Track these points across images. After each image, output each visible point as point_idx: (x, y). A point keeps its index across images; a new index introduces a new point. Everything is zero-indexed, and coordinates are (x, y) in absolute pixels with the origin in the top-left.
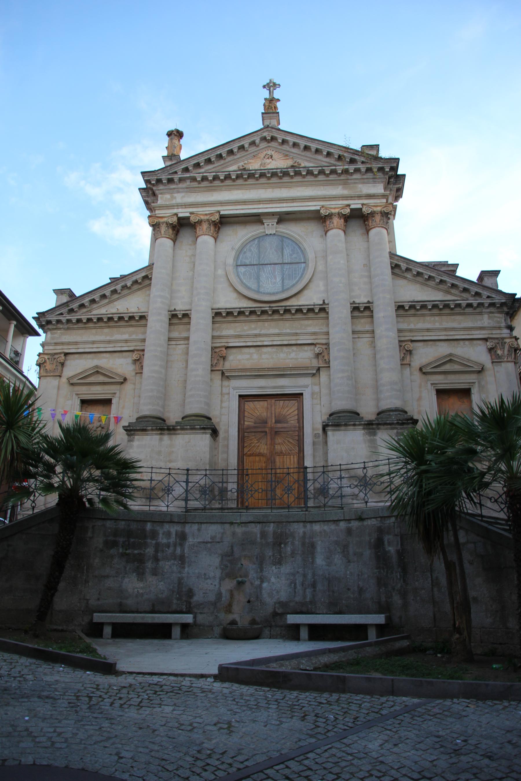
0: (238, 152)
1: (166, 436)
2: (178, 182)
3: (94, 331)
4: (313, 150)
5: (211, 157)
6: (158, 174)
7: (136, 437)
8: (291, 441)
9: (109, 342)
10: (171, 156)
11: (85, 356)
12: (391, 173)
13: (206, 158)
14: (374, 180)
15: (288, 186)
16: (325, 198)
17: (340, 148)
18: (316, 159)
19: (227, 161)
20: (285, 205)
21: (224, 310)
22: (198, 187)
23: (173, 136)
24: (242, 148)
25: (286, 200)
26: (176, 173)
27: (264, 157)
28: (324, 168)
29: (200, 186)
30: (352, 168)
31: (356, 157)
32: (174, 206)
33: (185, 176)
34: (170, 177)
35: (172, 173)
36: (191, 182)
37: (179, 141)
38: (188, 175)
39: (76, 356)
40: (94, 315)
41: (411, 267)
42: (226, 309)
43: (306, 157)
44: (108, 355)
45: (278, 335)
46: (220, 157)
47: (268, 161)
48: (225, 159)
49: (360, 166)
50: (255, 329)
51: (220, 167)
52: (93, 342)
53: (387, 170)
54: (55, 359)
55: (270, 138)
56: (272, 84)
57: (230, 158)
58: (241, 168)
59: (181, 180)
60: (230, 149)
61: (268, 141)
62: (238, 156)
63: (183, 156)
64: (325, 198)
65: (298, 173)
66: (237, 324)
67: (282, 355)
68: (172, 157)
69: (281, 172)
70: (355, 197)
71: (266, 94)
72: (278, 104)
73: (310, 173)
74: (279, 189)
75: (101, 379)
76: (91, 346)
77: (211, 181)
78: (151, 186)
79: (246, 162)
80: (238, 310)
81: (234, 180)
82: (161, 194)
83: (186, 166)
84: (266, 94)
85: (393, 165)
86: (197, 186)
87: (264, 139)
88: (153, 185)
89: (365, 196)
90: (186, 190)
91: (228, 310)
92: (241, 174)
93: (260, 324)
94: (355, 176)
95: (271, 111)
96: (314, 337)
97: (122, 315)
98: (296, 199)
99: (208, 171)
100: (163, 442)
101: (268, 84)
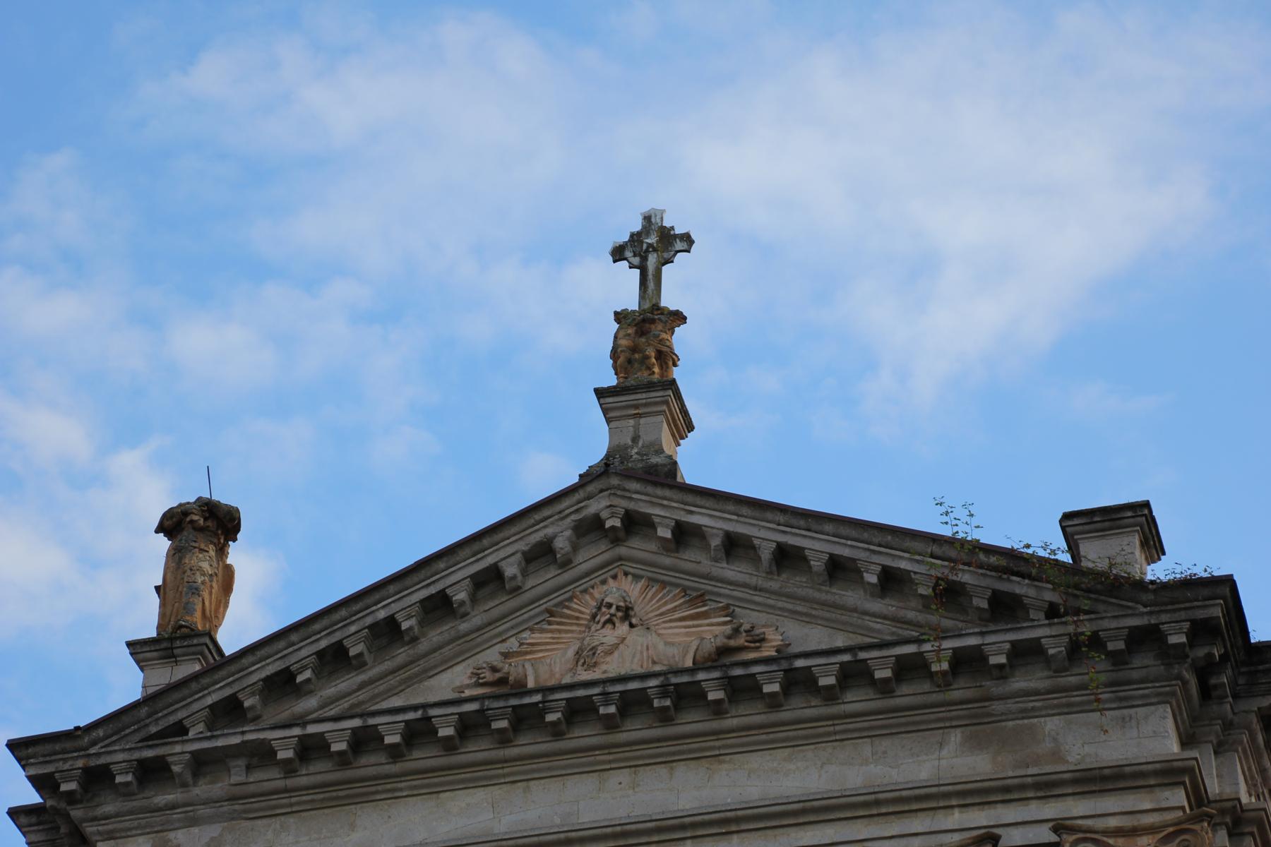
0: (474, 599)
2: (190, 779)
4: (817, 564)
5: (338, 639)
6: (94, 743)
10: (171, 639)
12: (1201, 652)
13: (323, 644)
14: (1123, 695)
15: (707, 750)
16: (878, 803)
17: (936, 549)
18: (835, 606)
19: (423, 646)
22: (286, 790)
23: (187, 533)
24: (490, 580)
25: (694, 826)
26: (180, 730)
27: (594, 616)
28: (862, 655)
29: (290, 782)
30: (997, 645)
31: (1019, 587)
33: (220, 743)
34: (149, 753)
35: (162, 734)
36: (249, 768)
37: (222, 551)
38: (236, 740)
46: (388, 632)
47: (608, 636)
48: (414, 640)
49: (1040, 631)
51: (362, 696)
53: (1177, 639)
55: (617, 523)
56: (652, 239)
57: (436, 635)
58: (489, 676)
59: (202, 764)
60: (433, 590)
61: (615, 538)
62: (477, 620)
63: (240, 627)
64: (878, 803)
65: (742, 690)
68: (179, 637)
69: (664, 691)
70: (1023, 787)
71: (624, 287)
72: (681, 339)
73: (799, 682)
74: (662, 771)
77: (343, 760)
78: (63, 805)
79: (513, 644)
81: (449, 746)
82: (110, 836)
83: (228, 692)
84: (624, 287)
85: (1201, 614)
86: (280, 784)
87: (591, 528)
88: (70, 797)
89: (1075, 782)
90: (226, 807)
92: (481, 712)
94: (1019, 683)
95: (643, 376)
98: (738, 820)
99: (326, 708)
101: (636, 238)
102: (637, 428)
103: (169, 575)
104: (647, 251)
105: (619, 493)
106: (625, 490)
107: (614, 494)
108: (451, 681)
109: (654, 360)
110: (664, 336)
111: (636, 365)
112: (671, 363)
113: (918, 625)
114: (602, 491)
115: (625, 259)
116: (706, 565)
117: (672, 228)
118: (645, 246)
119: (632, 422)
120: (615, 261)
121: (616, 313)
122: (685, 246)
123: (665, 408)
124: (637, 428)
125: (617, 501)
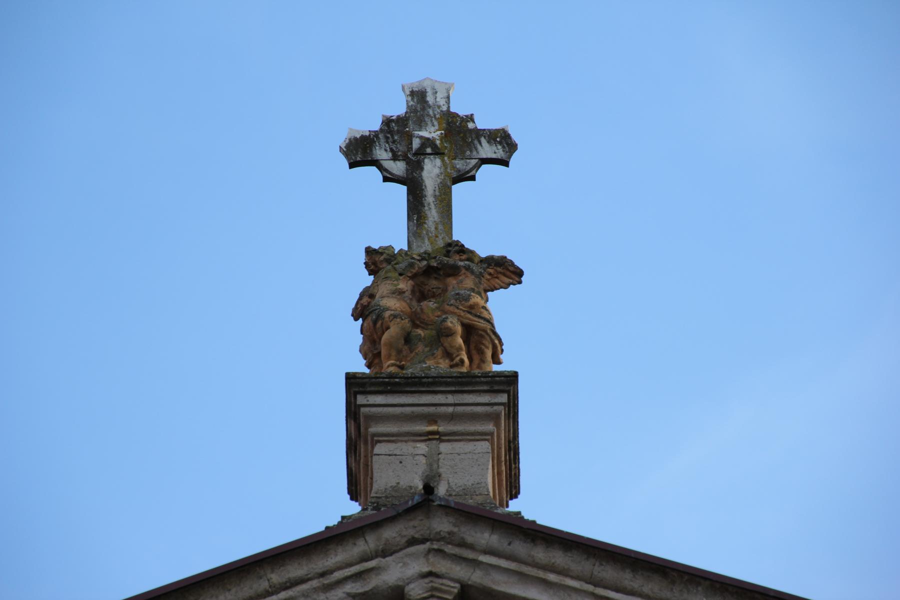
71: (381, 214)
84: (381, 214)
101: (394, 128)
102: (433, 460)
103: (411, 198)
104: (421, 152)
105: (449, 549)
106: (463, 544)
107: (439, 551)
109: (460, 341)
110: (476, 299)
111: (420, 348)
112: (489, 353)
114: (413, 542)
115: (376, 163)
117: (471, 118)
118: (416, 144)
119: (422, 448)
120: (352, 165)
121: (370, 252)
122: (497, 152)
123: (490, 427)
124: (433, 460)
125: (442, 566)
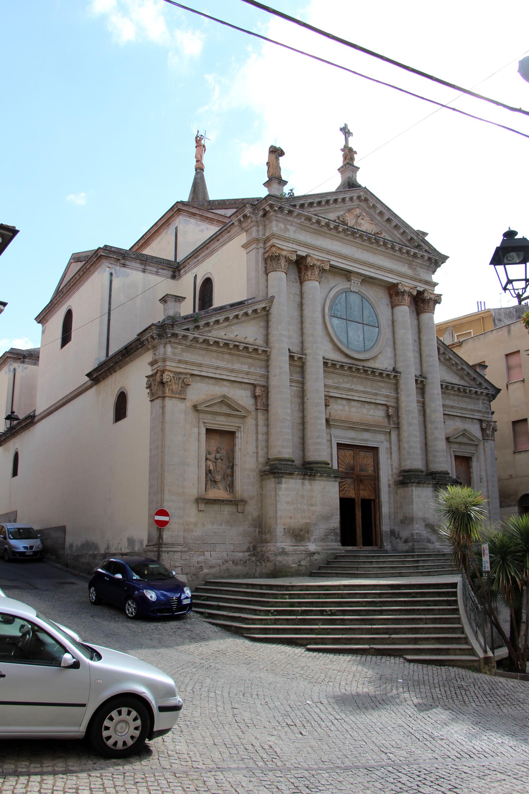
1: (307, 481)
3: (215, 354)
7: (284, 480)
8: (370, 487)
9: (232, 371)
11: (206, 380)
20: (372, 270)
21: (330, 362)
32: (290, 240)
39: (198, 378)
40: (222, 339)
41: (446, 352)
42: (332, 361)
43: (385, 227)
44: (228, 384)
45: (364, 392)
50: (347, 382)
52: (217, 368)
54: (180, 379)
58: (341, 219)
66: (334, 375)
67: (365, 411)
75: (224, 409)
76: (214, 371)
80: (341, 364)
86: (309, 225)
91: (334, 362)
93: (350, 378)
96: (386, 399)
97: (248, 346)
100: (305, 487)
108: (332, 216)
113: (403, 242)
116: (374, 214)
